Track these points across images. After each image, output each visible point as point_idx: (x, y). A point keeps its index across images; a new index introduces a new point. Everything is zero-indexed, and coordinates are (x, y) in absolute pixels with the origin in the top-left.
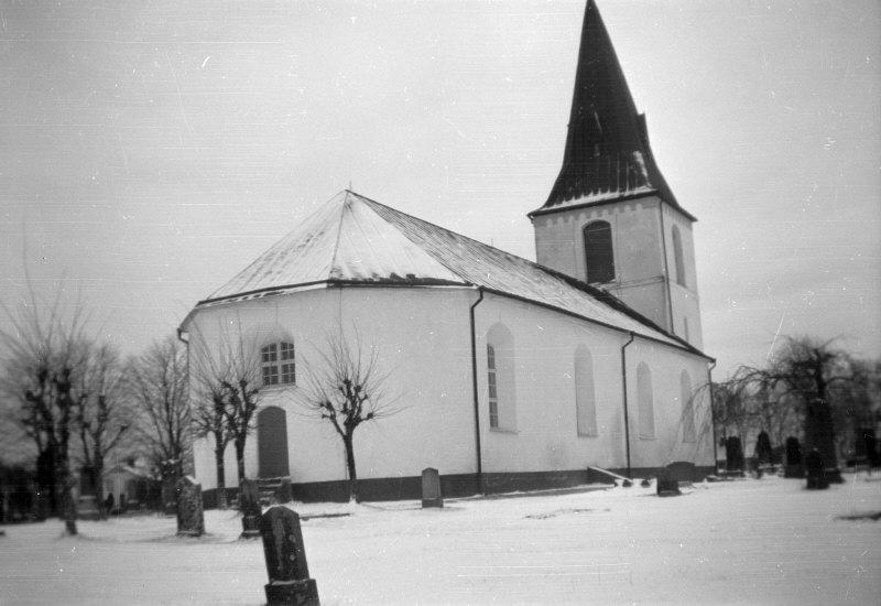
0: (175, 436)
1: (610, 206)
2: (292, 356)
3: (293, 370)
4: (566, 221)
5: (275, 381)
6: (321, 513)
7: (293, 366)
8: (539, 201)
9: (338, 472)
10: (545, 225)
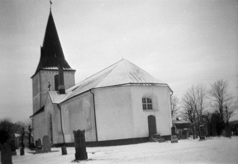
0: (172, 108)
1: (56, 71)
2: (143, 105)
3: (143, 108)
4: (50, 73)
5: (151, 105)
6: (89, 79)
7: (143, 102)
8: (34, 72)
9: (95, 140)
10: (44, 73)
